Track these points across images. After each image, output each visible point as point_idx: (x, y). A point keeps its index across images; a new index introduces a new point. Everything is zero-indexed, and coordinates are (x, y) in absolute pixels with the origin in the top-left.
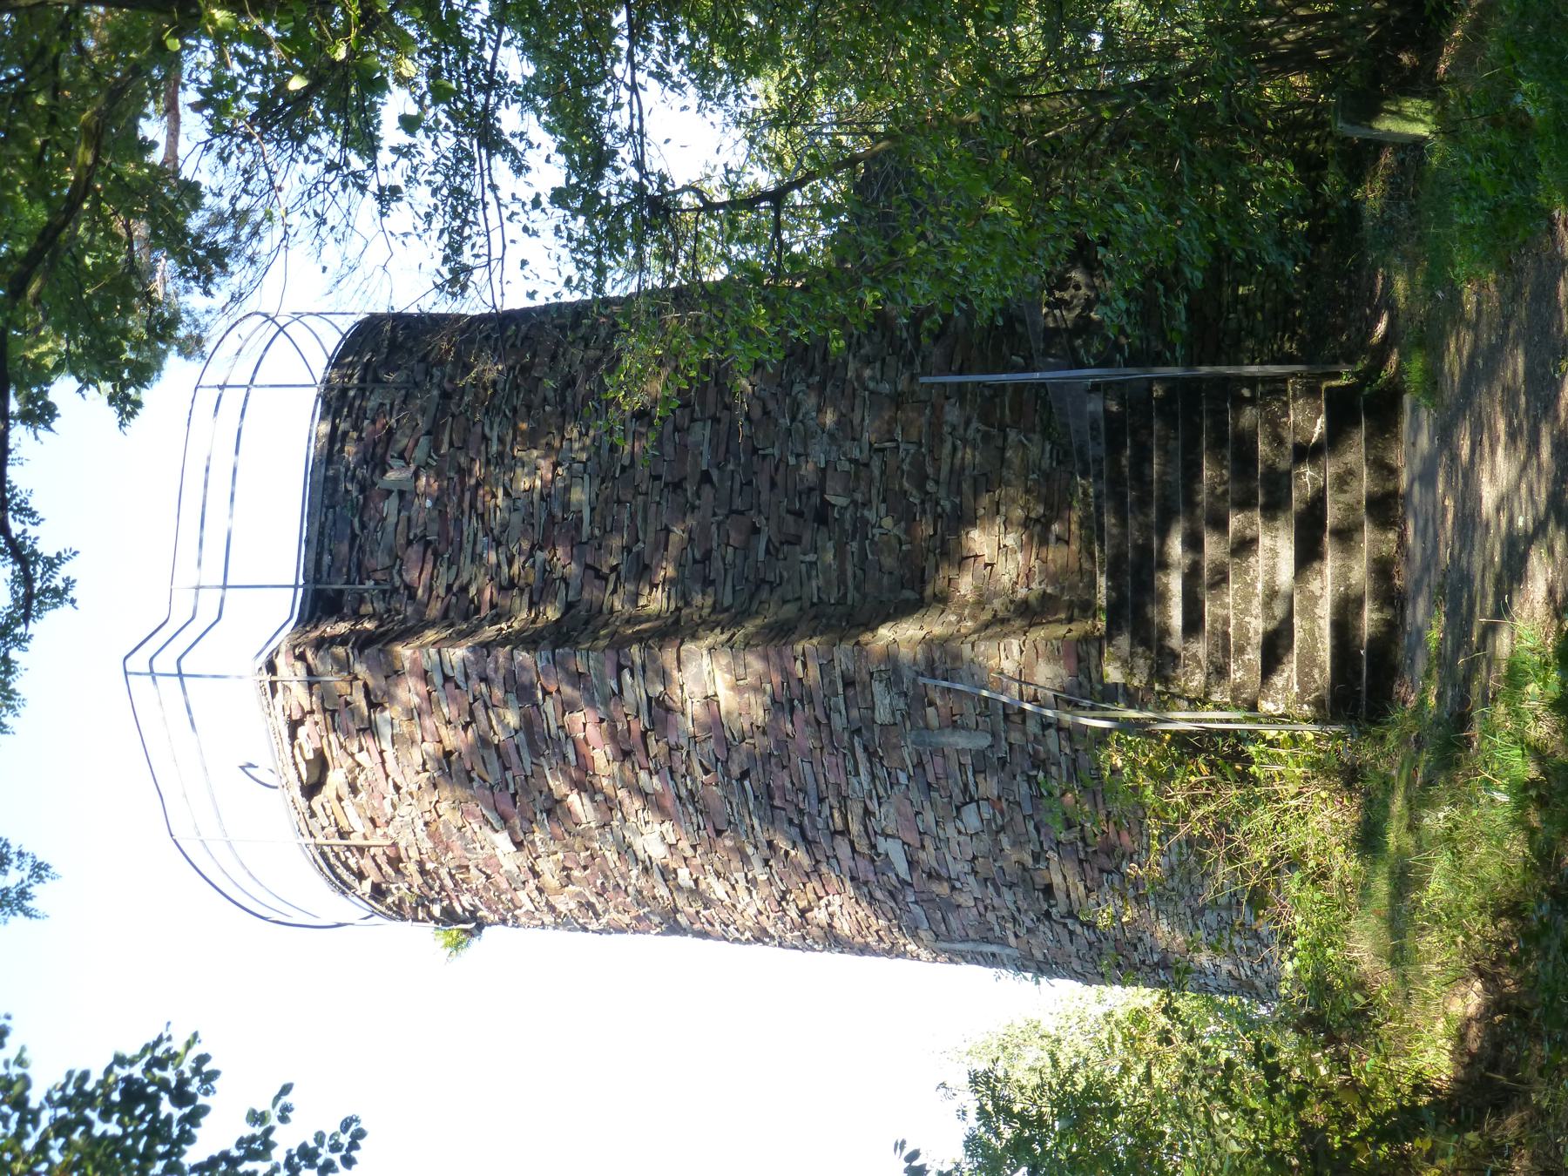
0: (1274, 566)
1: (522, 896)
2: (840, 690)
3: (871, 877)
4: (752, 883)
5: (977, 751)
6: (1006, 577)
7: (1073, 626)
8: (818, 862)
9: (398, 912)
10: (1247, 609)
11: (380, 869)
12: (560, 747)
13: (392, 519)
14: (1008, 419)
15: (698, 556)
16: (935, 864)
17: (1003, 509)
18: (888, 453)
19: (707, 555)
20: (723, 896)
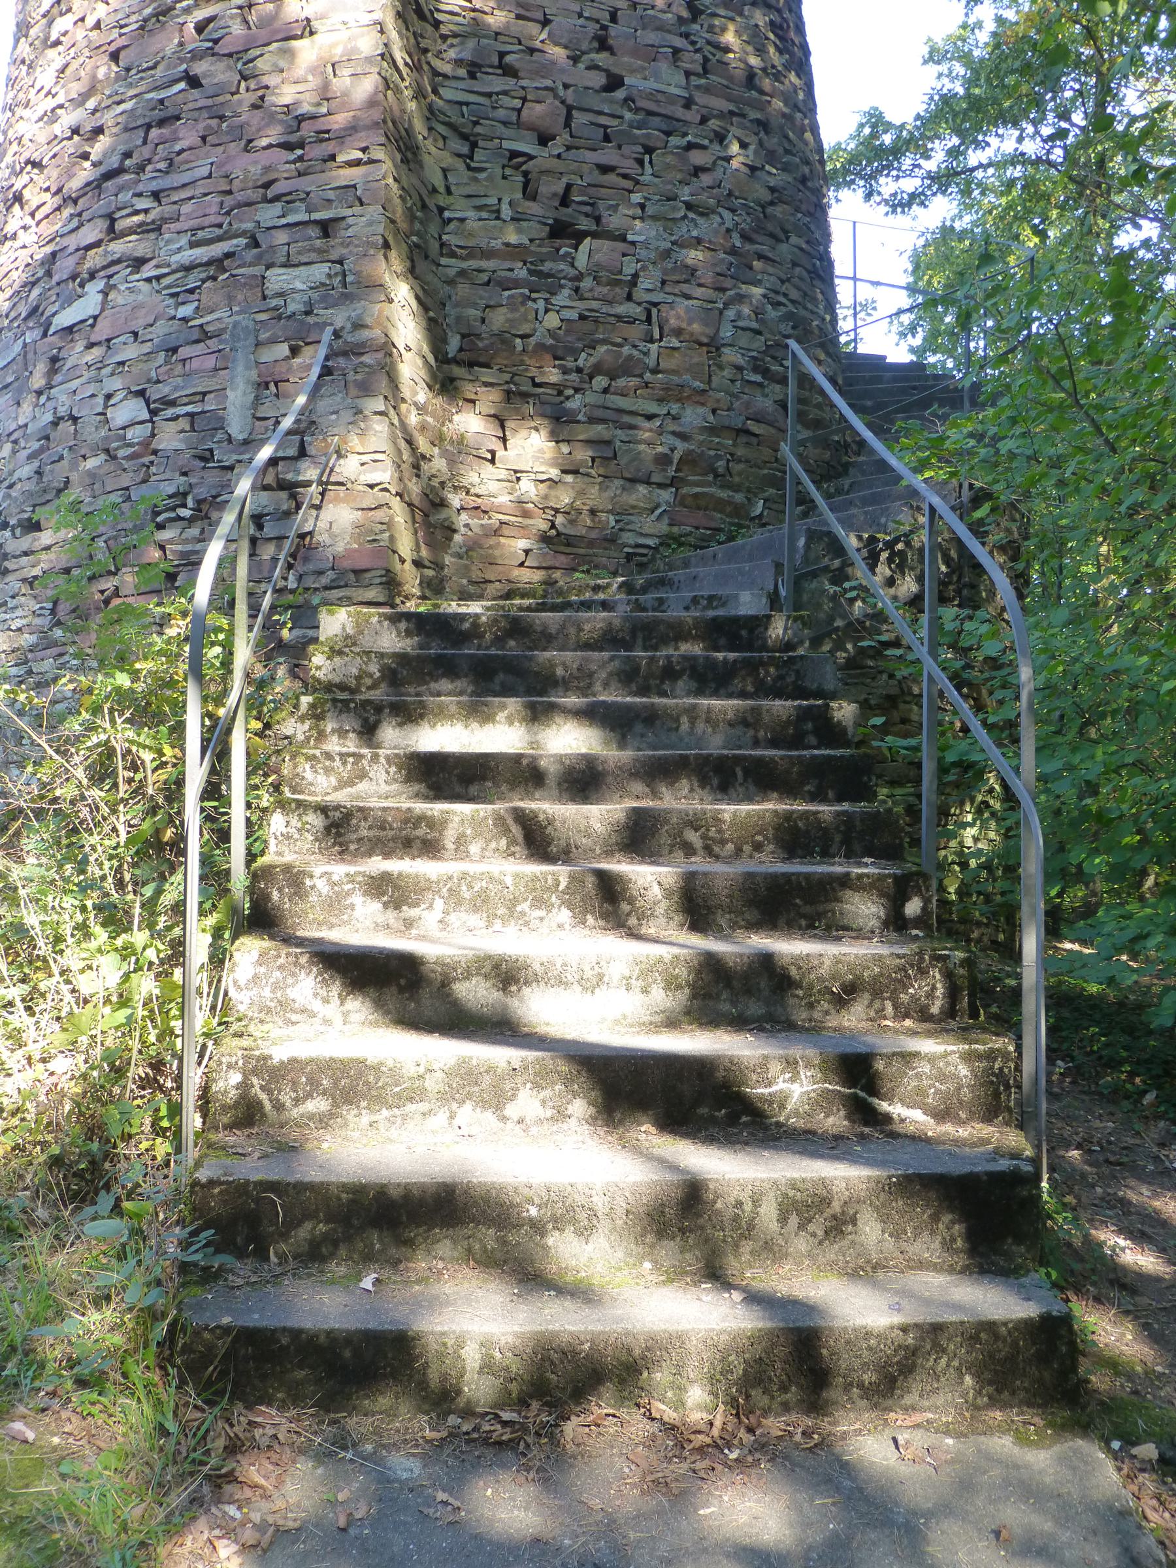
0: (562, 983)
3: (56, 278)
4: (51, 117)
5: (222, 419)
6: (476, 480)
7: (408, 566)
8: (75, 202)
10: (459, 903)
14: (685, 490)
15: (508, 59)
16: (69, 364)
17: (569, 478)
18: (645, 327)
19: (509, 71)
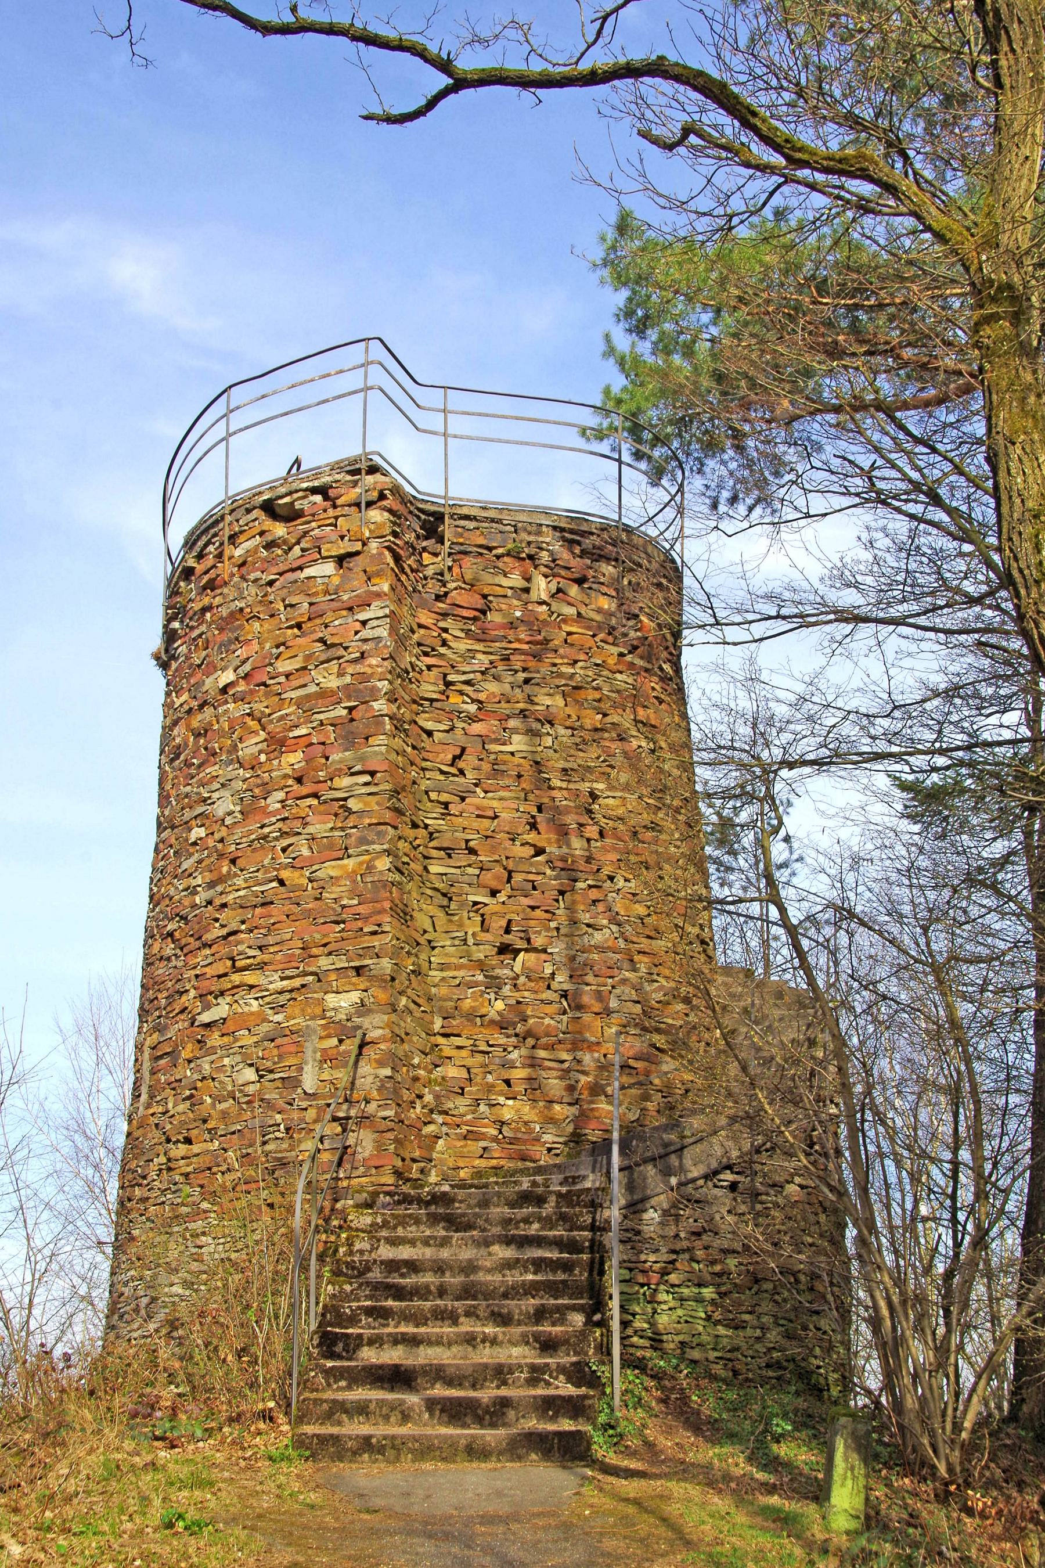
1: (185, 697)
2: (352, 964)
9: (173, 592)
11: (206, 572)
12: (305, 723)
13: (505, 582)
15: (471, 844)
20: (184, 866)
